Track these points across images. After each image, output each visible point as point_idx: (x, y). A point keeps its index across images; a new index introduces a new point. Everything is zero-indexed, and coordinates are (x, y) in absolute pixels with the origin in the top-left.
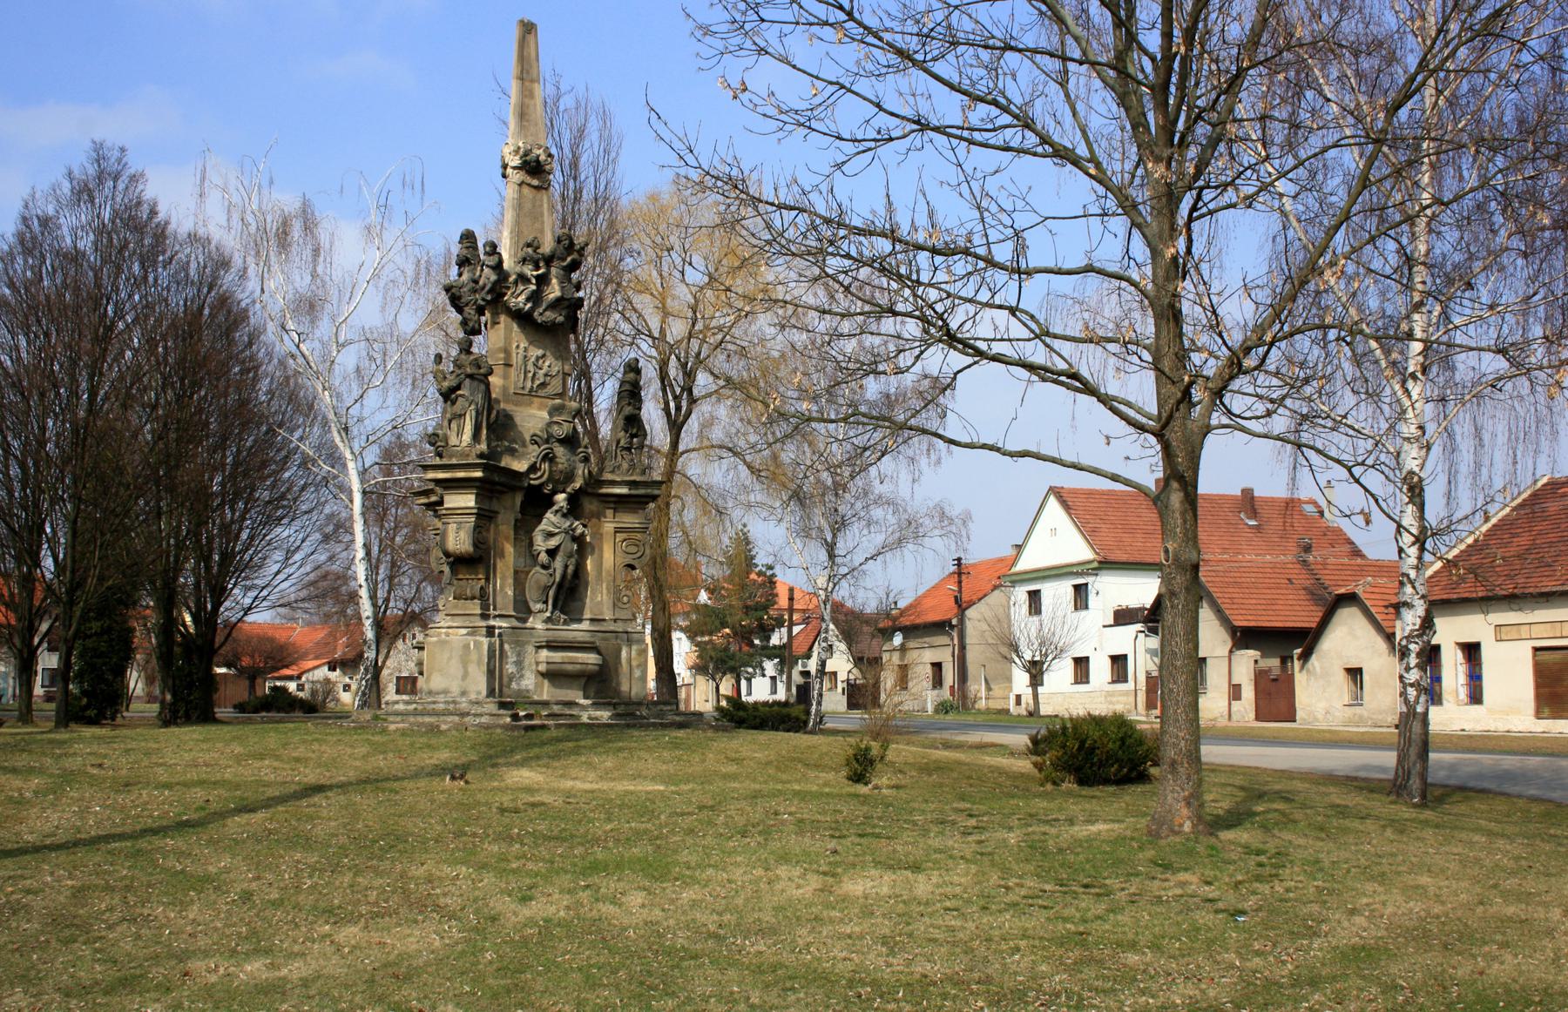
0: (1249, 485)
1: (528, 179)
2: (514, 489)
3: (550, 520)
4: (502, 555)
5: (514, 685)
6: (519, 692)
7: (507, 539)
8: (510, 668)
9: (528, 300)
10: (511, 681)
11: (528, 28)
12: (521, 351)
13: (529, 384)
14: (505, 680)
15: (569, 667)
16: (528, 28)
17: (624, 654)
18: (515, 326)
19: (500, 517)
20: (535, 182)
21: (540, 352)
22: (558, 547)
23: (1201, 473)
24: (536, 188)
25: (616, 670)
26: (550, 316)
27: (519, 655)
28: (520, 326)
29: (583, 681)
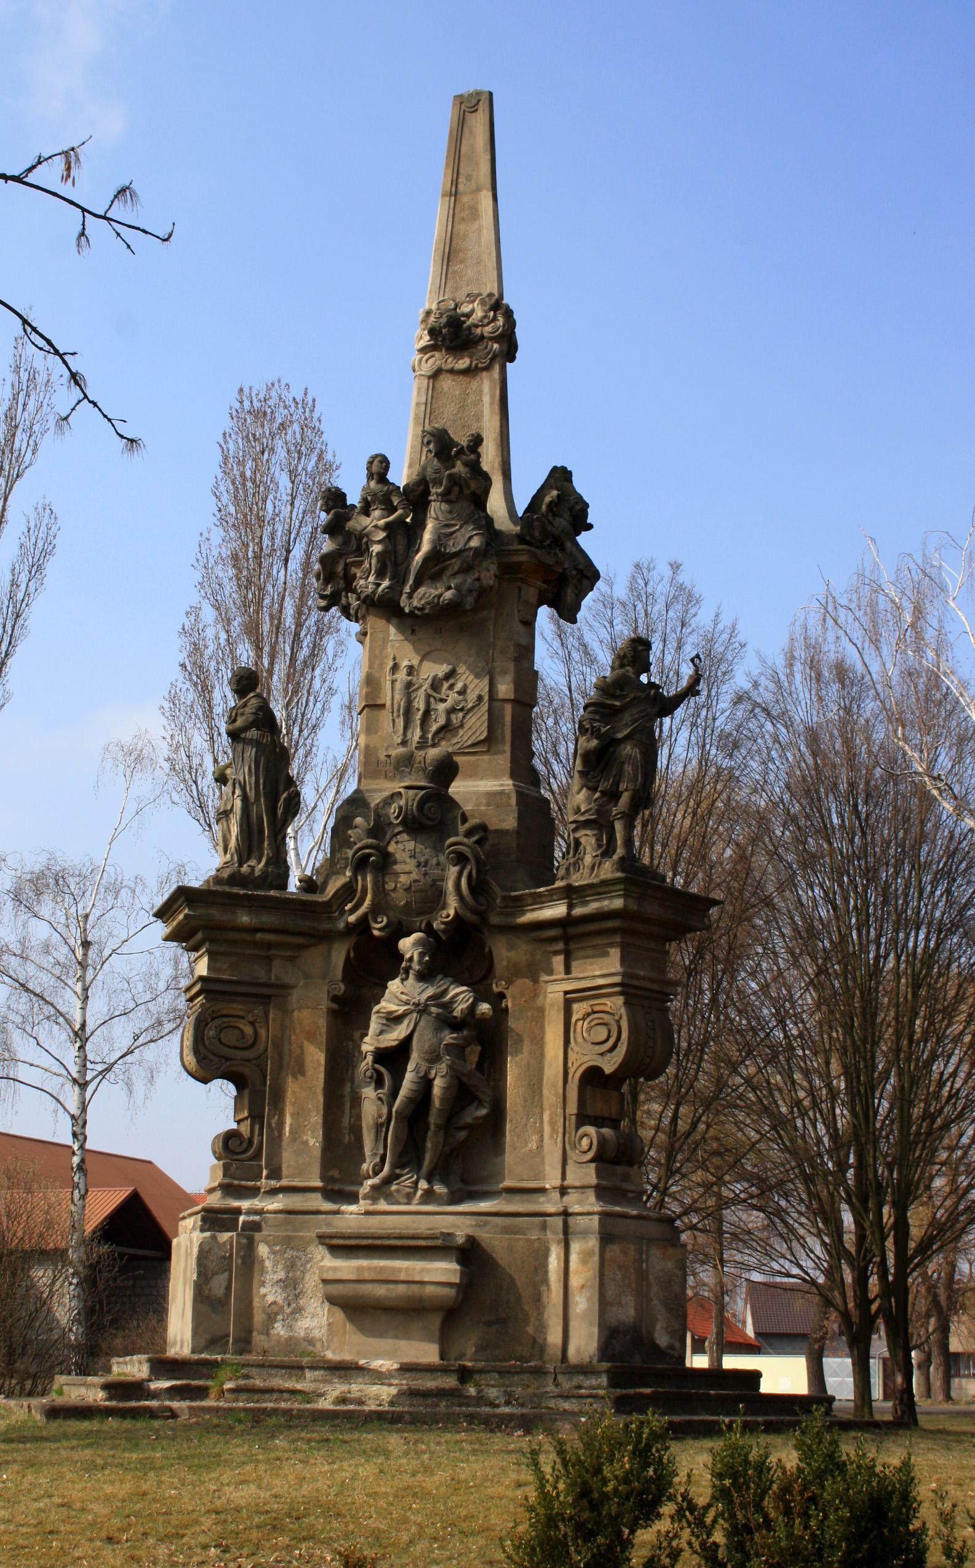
0: (127, 454)
1: (451, 363)
2: (327, 937)
3: (399, 993)
4: (300, 1070)
5: (279, 1329)
6: (291, 1344)
7: (311, 1036)
8: (269, 1293)
9: (380, 575)
10: (271, 1318)
11: (474, 106)
12: (402, 676)
13: (416, 734)
14: (258, 1317)
15: (380, 1291)
16: (474, 106)
17: (554, 1262)
18: (392, 630)
19: (295, 997)
20: (464, 363)
21: (442, 669)
22: (405, 1045)
23: (545, 477)
24: (467, 372)
25: (538, 1299)
26: (427, 593)
27: (291, 1266)
28: (400, 629)
29: (436, 1322)
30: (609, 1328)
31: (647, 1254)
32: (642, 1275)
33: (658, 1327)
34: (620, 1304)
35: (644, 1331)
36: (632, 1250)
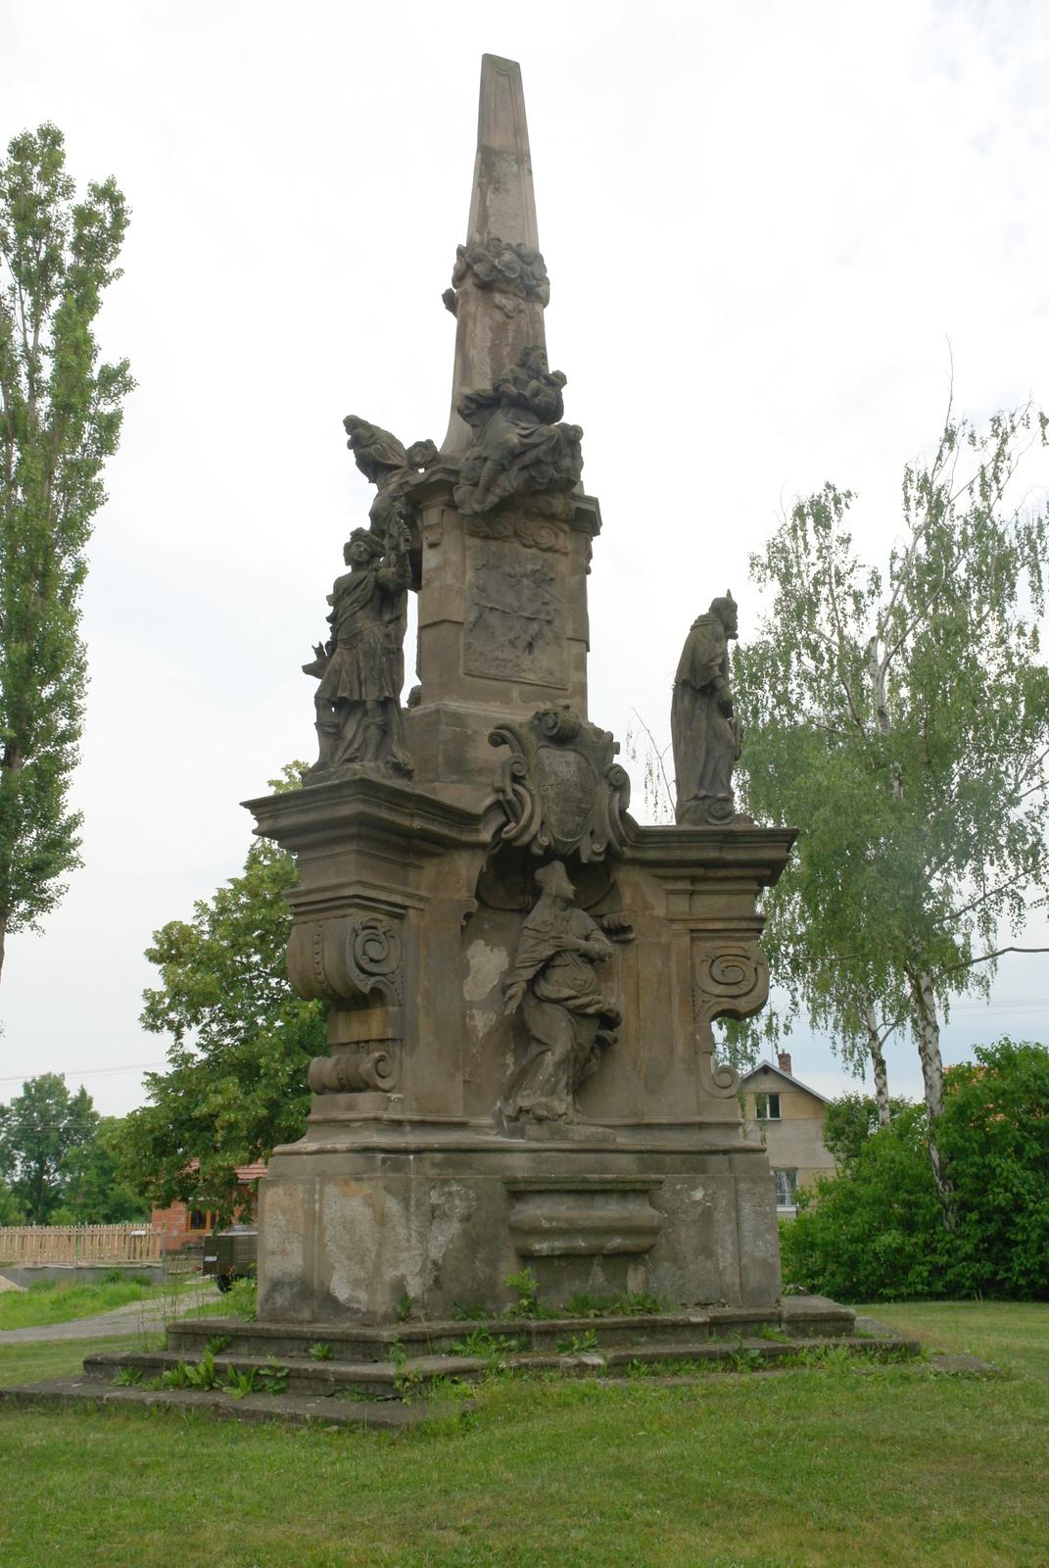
11: (501, 81)
16: (501, 81)
30: (271, 1279)
31: (322, 1191)
32: (314, 1219)
33: (335, 1278)
34: (284, 1252)
35: (316, 1281)
36: (300, 1192)
